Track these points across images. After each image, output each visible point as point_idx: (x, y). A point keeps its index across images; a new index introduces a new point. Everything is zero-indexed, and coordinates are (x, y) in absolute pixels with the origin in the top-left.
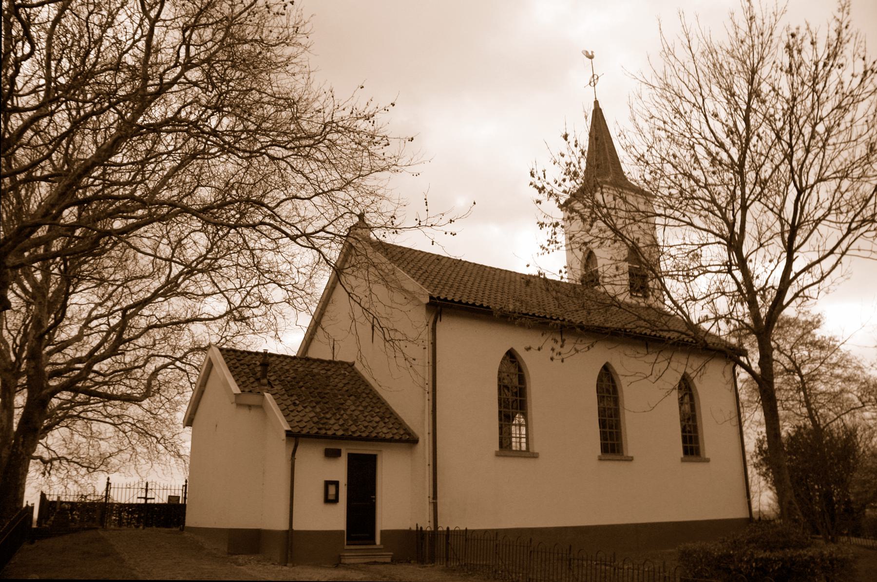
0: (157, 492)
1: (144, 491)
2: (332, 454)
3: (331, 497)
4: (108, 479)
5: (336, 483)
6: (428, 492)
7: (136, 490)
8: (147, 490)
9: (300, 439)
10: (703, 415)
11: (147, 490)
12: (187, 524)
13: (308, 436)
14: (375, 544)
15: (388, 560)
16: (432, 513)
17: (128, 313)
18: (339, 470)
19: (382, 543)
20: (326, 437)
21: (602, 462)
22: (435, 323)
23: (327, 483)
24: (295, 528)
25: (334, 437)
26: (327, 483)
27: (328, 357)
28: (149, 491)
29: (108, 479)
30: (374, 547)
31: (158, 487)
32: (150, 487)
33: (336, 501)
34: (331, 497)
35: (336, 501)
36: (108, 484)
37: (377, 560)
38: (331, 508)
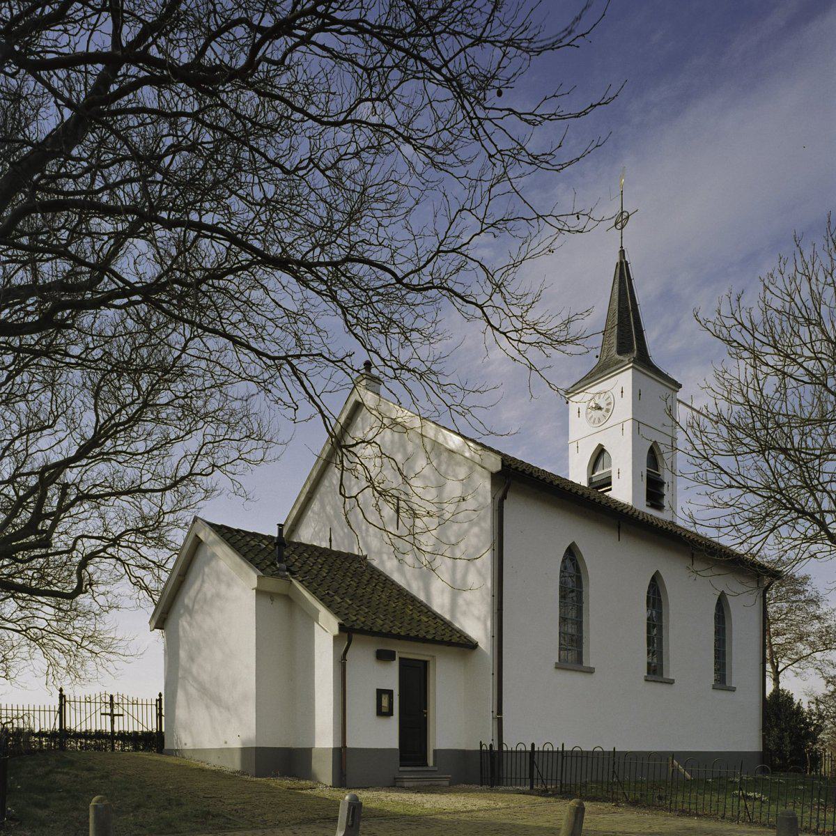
0: (125, 706)
1: (108, 706)
2: (384, 656)
3: (384, 710)
4: (61, 690)
5: (390, 693)
6: (490, 705)
7: (98, 705)
8: (112, 705)
9: (354, 636)
10: (735, 635)
11: (112, 705)
12: (166, 747)
13: (362, 631)
14: (427, 765)
15: (447, 783)
16: (496, 732)
17: (47, 475)
18: (390, 677)
19: (435, 764)
20: (379, 634)
21: (647, 683)
22: (504, 497)
23: (380, 693)
24: (349, 745)
25: (389, 635)
26: (380, 693)
27: (325, 545)
28: (115, 706)
29: (61, 690)
30: (425, 769)
31: (125, 701)
32: (115, 700)
33: (390, 713)
34: (384, 710)
35: (390, 713)
36: (62, 697)
37: (433, 783)
38: (383, 721)
